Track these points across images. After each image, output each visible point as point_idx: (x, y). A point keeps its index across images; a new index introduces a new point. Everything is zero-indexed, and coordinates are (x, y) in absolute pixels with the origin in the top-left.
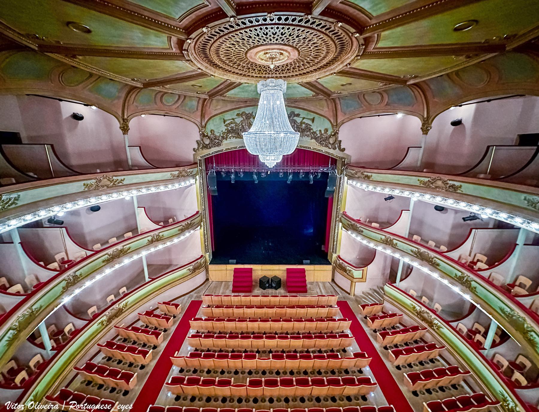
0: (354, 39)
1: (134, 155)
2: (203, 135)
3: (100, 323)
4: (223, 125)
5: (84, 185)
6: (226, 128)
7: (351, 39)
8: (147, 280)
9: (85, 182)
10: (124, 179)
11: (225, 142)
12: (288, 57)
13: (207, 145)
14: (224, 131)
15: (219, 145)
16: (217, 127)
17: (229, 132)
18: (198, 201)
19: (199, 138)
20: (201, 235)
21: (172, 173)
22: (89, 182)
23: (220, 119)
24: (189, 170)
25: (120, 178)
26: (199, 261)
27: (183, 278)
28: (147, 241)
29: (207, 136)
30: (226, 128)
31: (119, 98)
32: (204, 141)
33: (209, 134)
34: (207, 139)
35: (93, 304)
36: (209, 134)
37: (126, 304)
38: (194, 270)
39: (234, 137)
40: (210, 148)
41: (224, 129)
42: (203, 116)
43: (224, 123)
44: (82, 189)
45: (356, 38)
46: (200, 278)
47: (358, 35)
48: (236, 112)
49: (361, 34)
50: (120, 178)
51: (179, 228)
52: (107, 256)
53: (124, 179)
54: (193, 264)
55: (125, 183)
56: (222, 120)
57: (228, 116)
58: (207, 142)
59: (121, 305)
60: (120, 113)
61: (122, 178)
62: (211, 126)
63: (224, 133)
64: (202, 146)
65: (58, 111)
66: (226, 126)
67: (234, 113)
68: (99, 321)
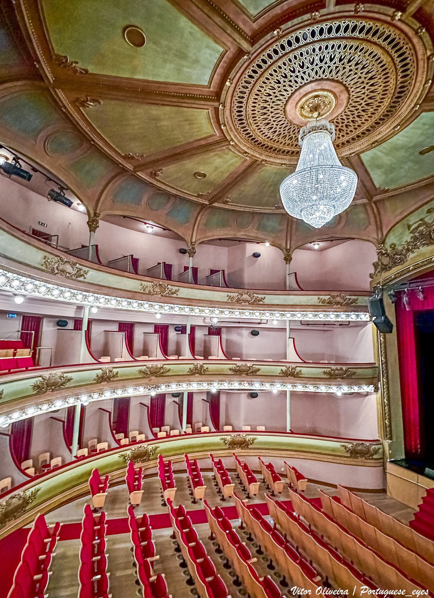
0: (399, 24)
1: (290, 281)
2: (380, 254)
3: (223, 439)
4: (407, 232)
5: (228, 296)
6: (412, 235)
7: (394, 26)
8: (288, 431)
9: (229, 294)
10: (265, 298)
11: (411, 255)
12: (345, 112)
13: (386, 265)
14: (409, 241)
15: (402, 261)
16: (399, 238)
17: (415, 239)
18: (374, 348)
19: (376, 260)
20: (377, 404)
21: (321, 297)
22: (232, 294)
23: (404, 225)
24: (348, 297)
25: (260, 296)
26: (368, 444)
27: (332, 456)
28: (280, 371)
29: (385, 253)
30: (412, 235)
31: (281, 231)
32: (383, 261)
33: (389, 250)
34: (390, 258)
35: (305, 477)
36: (389, 250)
37: (254, 439)
38: (354, 453)
39: (424, 245)
40: (390, 268)
41: (408, 237)
42: (379, 227)
43: (409, 229)
44: (226, 299)
45: (399, 20)
46: (366, 476)
47: (400, 14)
48: (426, 208)
49: (403, 10)
50: (260, 296)
51: (325, 370)
52: (235, 366)
53: (265, 298)
54: (355, 443)
55: (266, 301)
56: (406, 226)
57: (413, 220)
58: (386, 261)
59: (248, 438)
60: (284, 245)
61: (263, 296)
62: (391, 240)
63: (408, 244)
64: (381, 267)
65: (244, 250)
66: (411, 233)
67: (422, 210)
68: (223, 437)
